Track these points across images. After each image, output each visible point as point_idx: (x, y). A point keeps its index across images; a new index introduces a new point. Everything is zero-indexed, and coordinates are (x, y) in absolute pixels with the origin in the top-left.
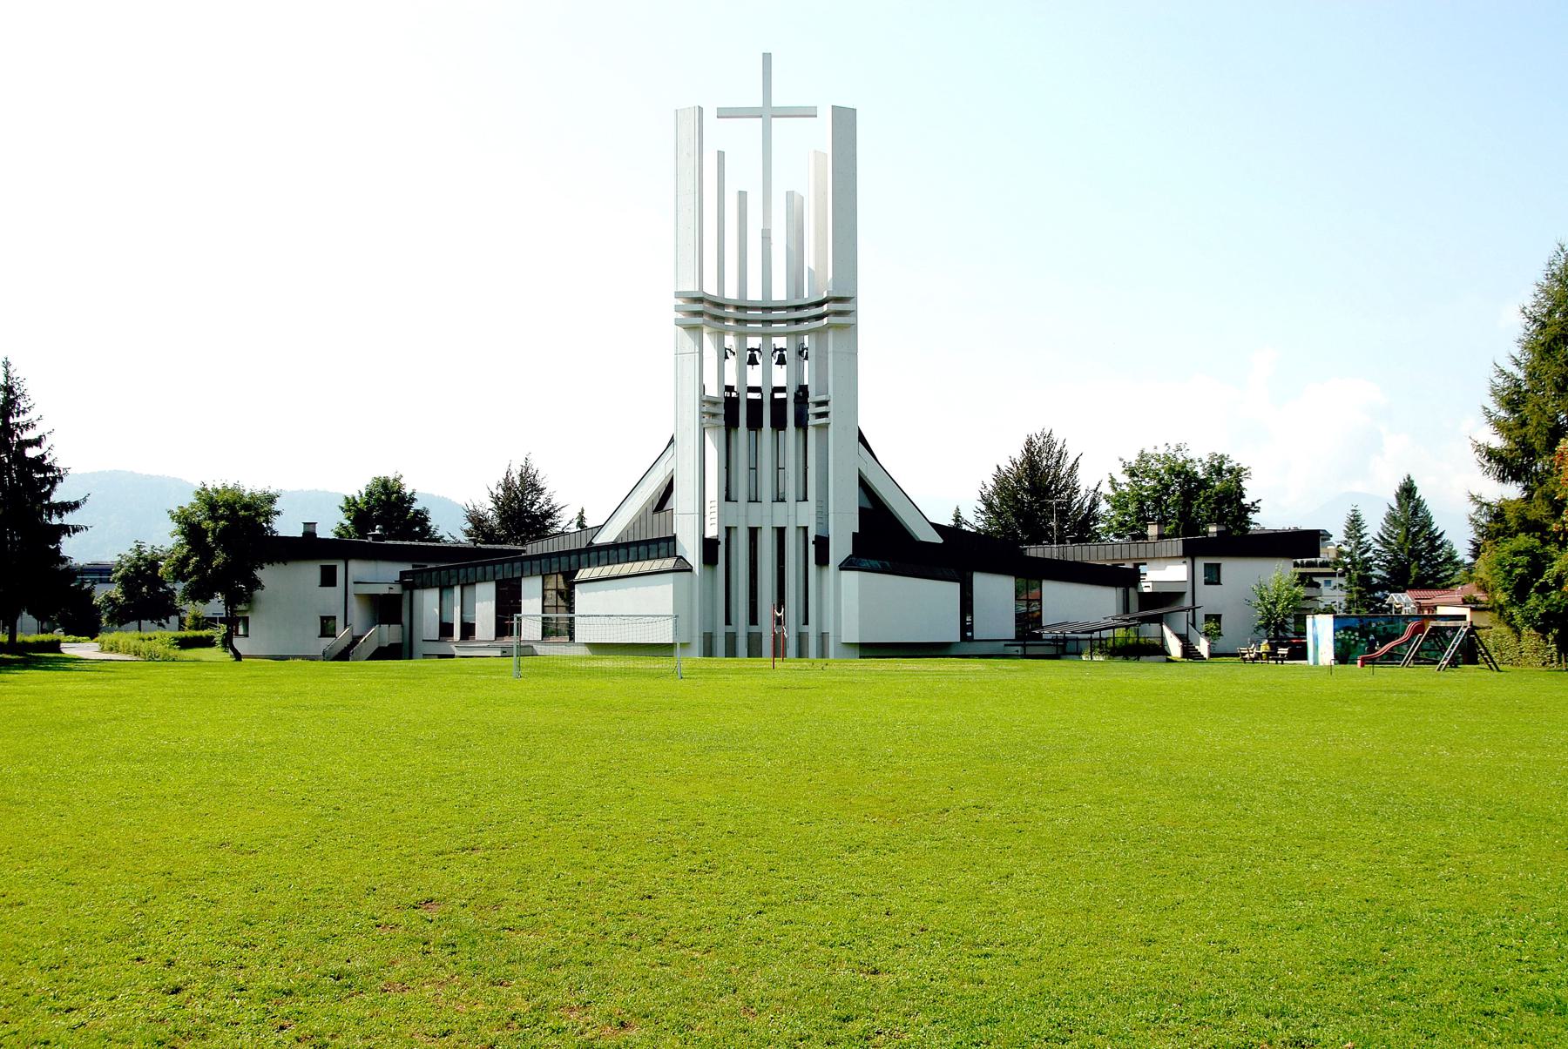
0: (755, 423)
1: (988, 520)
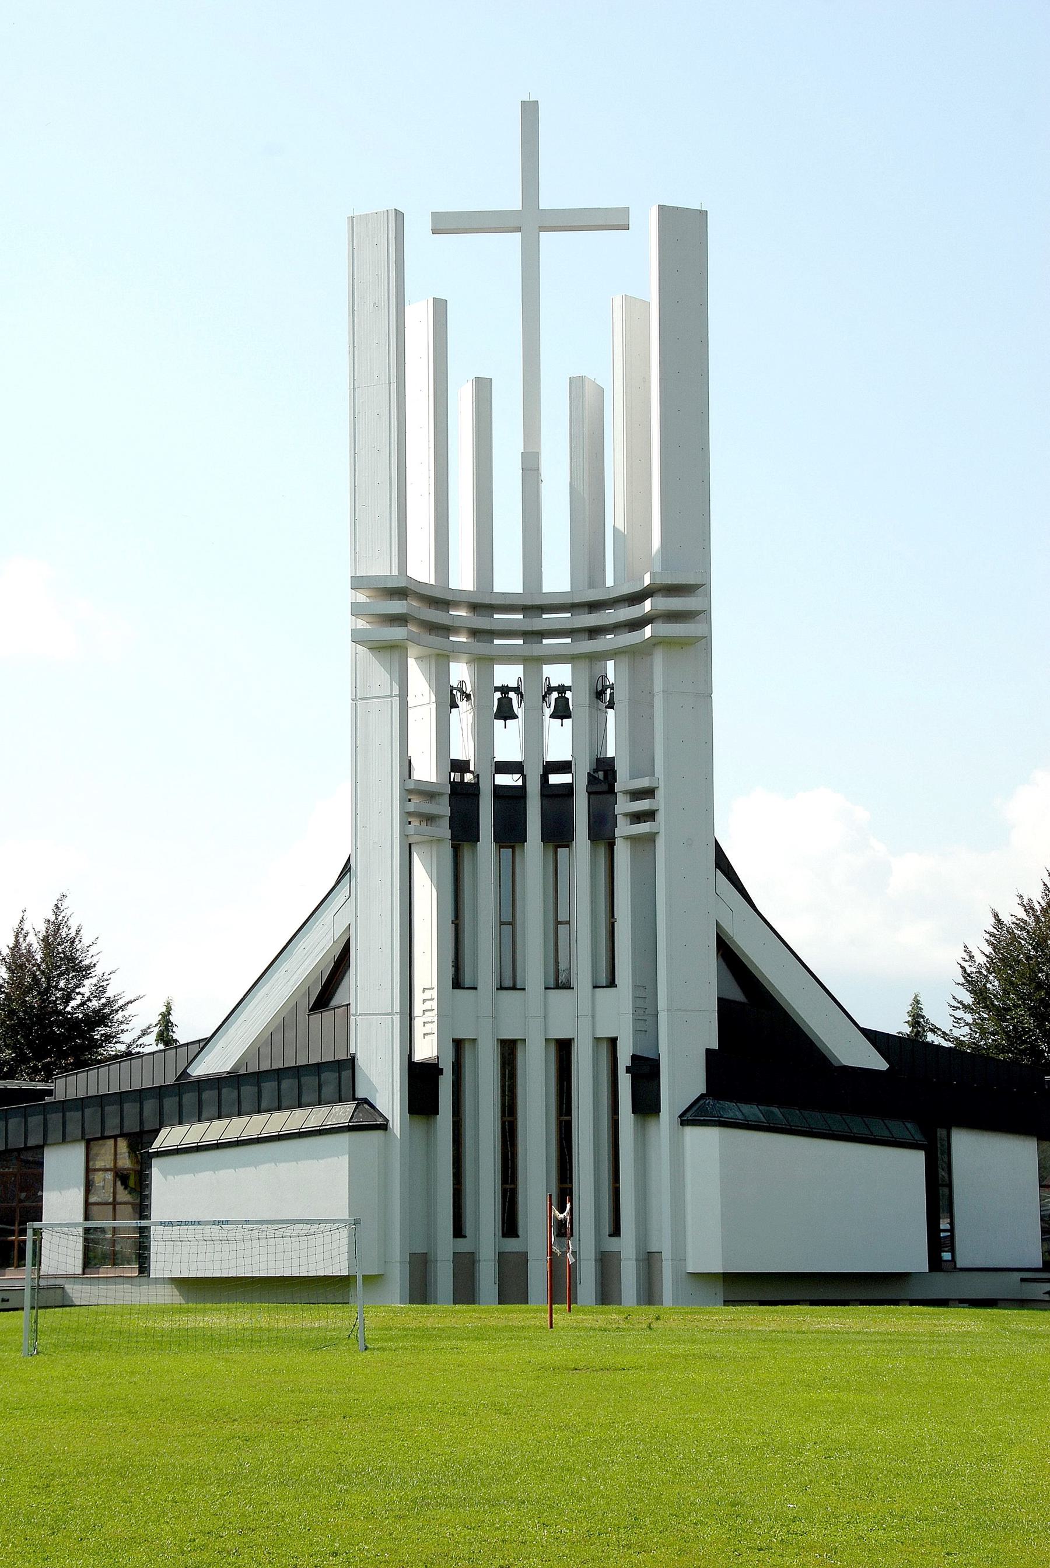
0: (511, 834)
1: (979, 1026)
